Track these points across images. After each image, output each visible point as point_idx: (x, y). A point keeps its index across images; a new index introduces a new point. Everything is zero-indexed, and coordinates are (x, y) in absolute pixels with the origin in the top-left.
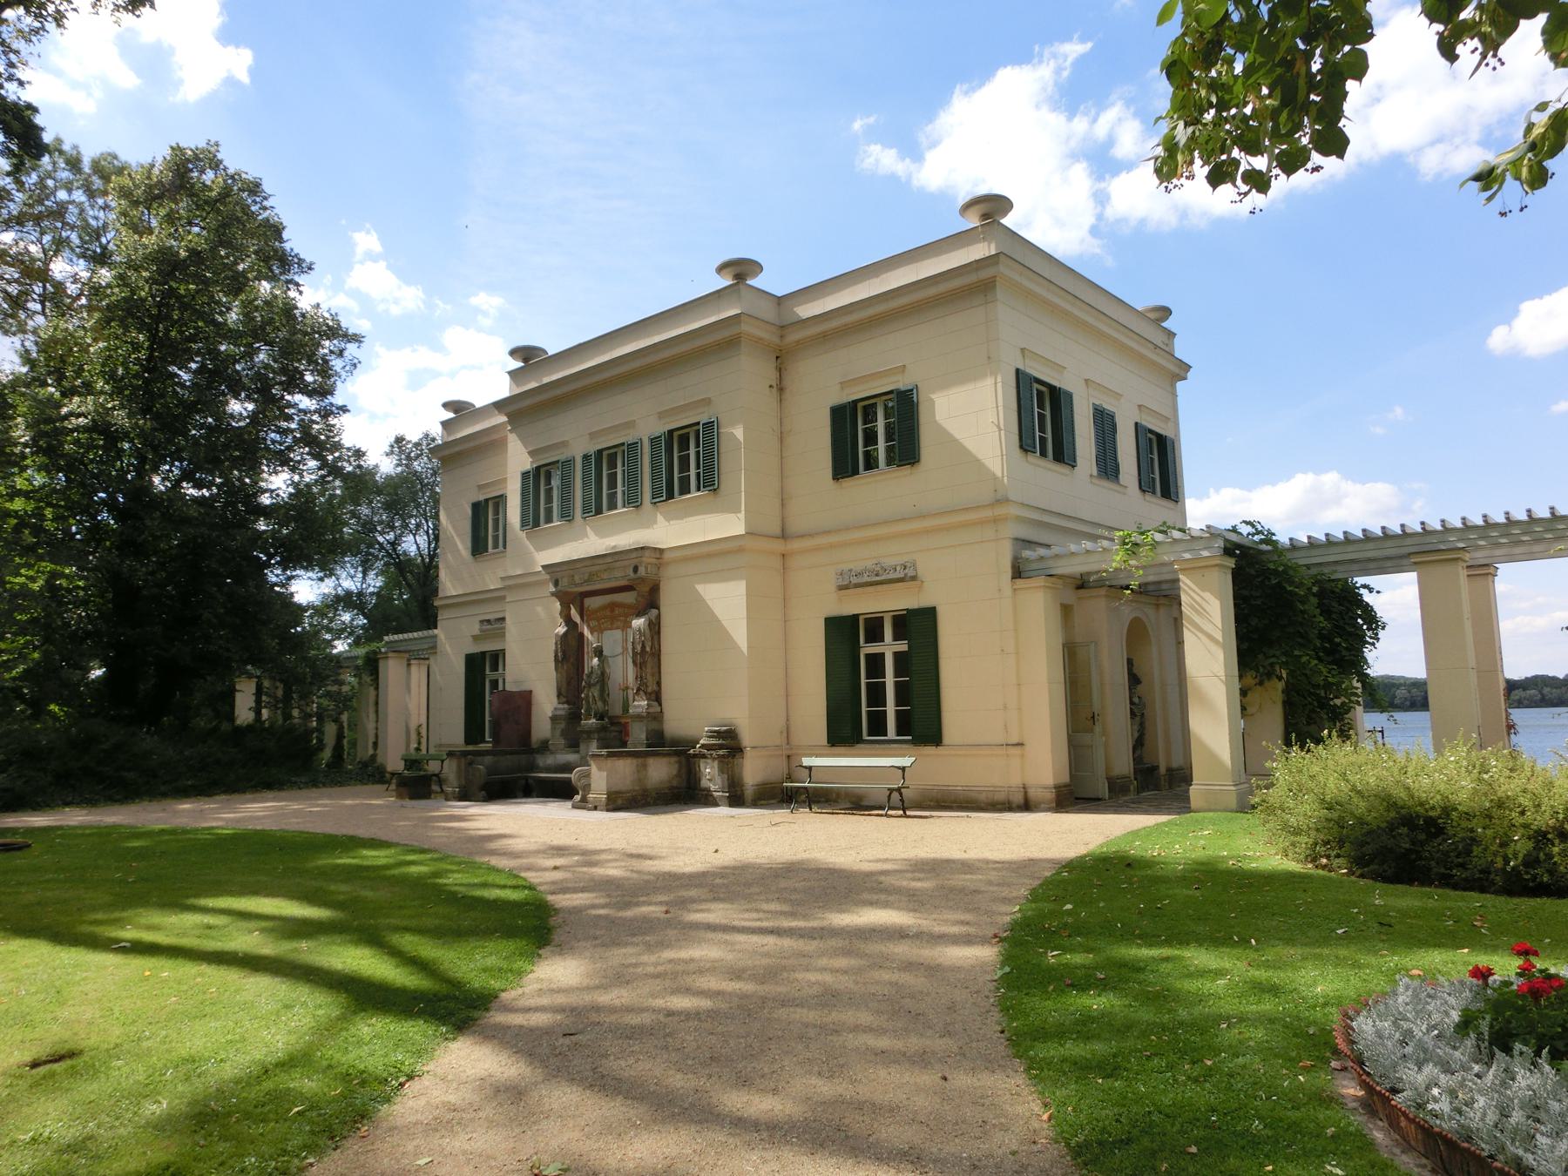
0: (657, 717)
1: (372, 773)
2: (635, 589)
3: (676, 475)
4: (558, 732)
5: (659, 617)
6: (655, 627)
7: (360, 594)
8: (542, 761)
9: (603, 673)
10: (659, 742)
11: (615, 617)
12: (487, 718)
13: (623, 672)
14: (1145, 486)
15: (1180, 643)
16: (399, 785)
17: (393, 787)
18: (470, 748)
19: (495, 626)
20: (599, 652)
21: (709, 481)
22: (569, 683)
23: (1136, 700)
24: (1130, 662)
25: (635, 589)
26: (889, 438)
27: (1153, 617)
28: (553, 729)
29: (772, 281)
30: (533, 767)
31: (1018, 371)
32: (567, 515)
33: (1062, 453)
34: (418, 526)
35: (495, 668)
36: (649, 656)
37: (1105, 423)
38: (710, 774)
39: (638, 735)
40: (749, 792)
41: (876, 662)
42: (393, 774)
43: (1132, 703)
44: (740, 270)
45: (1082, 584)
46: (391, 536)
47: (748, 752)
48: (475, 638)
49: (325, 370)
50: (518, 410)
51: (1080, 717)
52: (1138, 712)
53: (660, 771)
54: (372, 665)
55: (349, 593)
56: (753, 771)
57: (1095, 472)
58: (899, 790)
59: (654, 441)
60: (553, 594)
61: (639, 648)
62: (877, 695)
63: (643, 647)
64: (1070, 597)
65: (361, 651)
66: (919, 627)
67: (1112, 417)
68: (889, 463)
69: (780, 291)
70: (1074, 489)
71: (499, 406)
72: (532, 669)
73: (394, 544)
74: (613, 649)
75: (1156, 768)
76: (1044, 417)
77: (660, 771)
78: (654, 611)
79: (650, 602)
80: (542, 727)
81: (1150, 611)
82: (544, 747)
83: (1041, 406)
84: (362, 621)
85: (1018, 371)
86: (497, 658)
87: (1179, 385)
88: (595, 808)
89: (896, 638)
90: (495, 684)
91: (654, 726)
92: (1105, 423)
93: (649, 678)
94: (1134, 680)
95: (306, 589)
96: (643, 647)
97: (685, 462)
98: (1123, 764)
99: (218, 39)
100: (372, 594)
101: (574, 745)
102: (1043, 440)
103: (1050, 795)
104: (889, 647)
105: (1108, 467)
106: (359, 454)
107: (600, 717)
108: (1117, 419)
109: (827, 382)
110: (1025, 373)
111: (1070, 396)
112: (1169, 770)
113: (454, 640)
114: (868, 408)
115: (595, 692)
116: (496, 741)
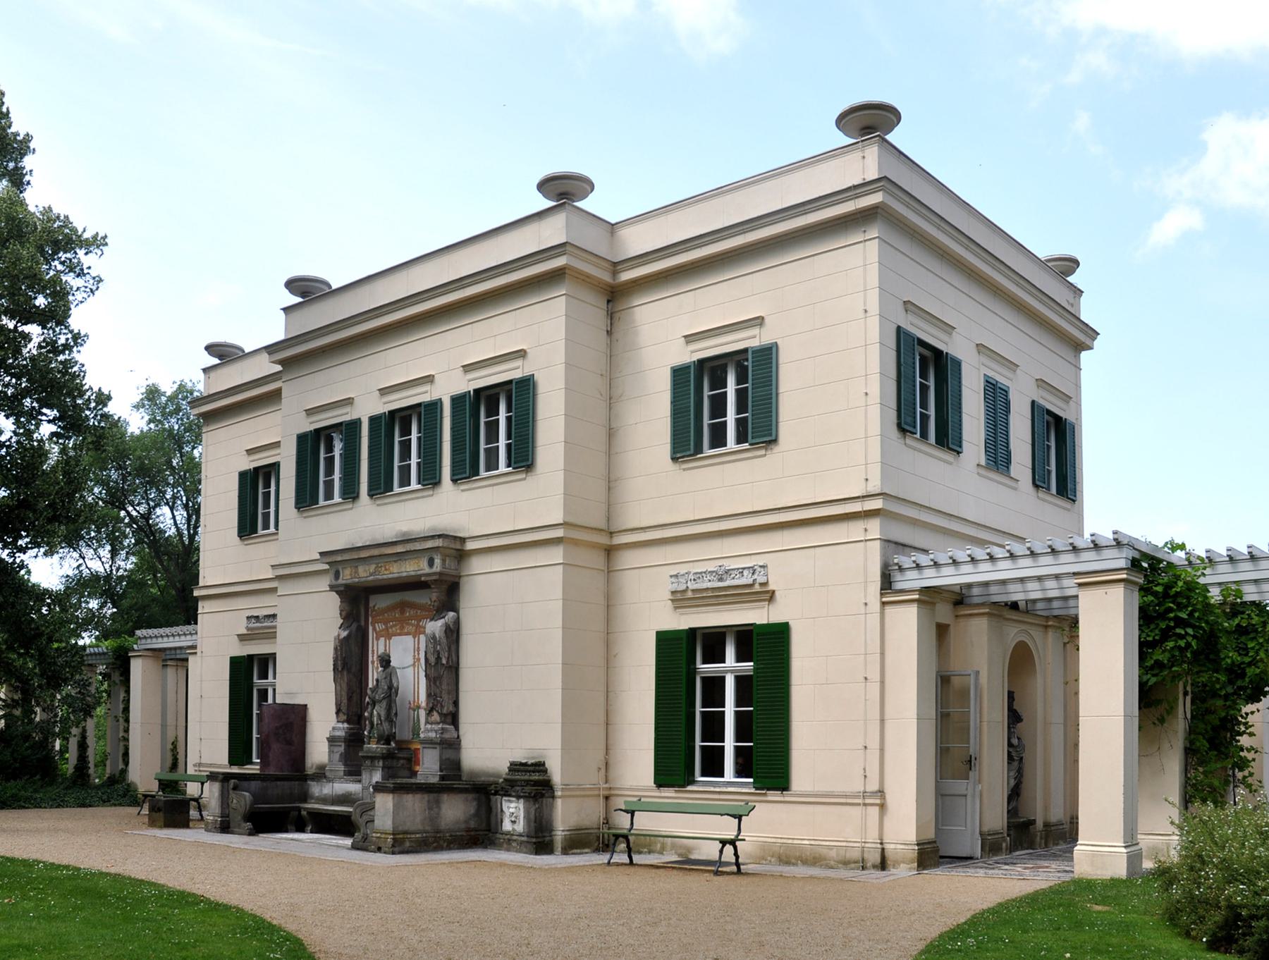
0: (451, 746)
1: (117, 791)
2: (428, 586)
4: (337, 756)
5: (457, 622)
6: (453, 633)
7: (108, 577)
8: (317, 789)
9: (390, 687)
10: (454, 777)
11: (405, 619)
12: (255, 735)
13: (413, 682)
14: (1039, 482)
16: (152, 809)
17: (145, 811)
18: (235, 770)
19: (262, 627)
20: (385, 661)
21: (522, 458)
22: (350, 699)
23: (1015, 741)
24: (1011, 696)
27: (1046, 646)
28: (331, 752)
30: (305, 797)
31: (899, 328)
32: (350, 493)
33: (948, 439)
34: (174, 497)
35: (264, 675)
36: (445, 669)
37: (996, 397)
38: (513, 815)
39: (429, 766)
41: (714, 687)
42: (146, 796)
43: (1010, 745)
44: (564, 189)
45: (959, 598)
46: (143, 509)
48: (242, 638)
49: (60, 295)
50: (296, 356)
51: (949, 755)
52: (1016, 756)
53: (455, 811)
54: (121, 663)
55: (95, 577)
56: (564, 816)
57: (983, 463)
58: (733, 842)
60: (332, 588)
61: (432, 660)
62: (714, 727)
63: (438, 659)
64: (944, 612)
65: (106, 645)
66: (768, 647)
67: (1006, 392)
68: (741, 438)
69: (613, 222)
70: (957, 483)
71: (271, 349)
72: (306, 678)
73: (146, 517)
74: (404, 655)
75: (1033, 822)
76: (925, 387)
77: (455, 811)
78: (451, 614)
79: (447, 593)
80: (319, 750)
81: (1036, 633)
82: (321, 774)
83: (924, 375)
84: (109, 610)
86: (265, 663)
87: (1084, 355)
88: (379, 849)
89: (740, 658)
90: (263, 694)
91: (449, 754)
92: (996, 397)
93: (445, 696)
94: (1014, 717)
95: (47, 570)
96: (438, 659)
97: (493, 425)
98: (997, 818)
99: (774, 441)
100: (121, 578)
101: (354, 772)
102: (925, 418)
103: (912, 851)
104: (731, 665)
105: (998, 457)
106: (103, 399)
107: (387, 739)
108: (1011, 396)
109: (670, 332)
110: (908, 334)
111: (957, 364)
112: (1047, 825)
113: (215, 639)
116: (264, 764)
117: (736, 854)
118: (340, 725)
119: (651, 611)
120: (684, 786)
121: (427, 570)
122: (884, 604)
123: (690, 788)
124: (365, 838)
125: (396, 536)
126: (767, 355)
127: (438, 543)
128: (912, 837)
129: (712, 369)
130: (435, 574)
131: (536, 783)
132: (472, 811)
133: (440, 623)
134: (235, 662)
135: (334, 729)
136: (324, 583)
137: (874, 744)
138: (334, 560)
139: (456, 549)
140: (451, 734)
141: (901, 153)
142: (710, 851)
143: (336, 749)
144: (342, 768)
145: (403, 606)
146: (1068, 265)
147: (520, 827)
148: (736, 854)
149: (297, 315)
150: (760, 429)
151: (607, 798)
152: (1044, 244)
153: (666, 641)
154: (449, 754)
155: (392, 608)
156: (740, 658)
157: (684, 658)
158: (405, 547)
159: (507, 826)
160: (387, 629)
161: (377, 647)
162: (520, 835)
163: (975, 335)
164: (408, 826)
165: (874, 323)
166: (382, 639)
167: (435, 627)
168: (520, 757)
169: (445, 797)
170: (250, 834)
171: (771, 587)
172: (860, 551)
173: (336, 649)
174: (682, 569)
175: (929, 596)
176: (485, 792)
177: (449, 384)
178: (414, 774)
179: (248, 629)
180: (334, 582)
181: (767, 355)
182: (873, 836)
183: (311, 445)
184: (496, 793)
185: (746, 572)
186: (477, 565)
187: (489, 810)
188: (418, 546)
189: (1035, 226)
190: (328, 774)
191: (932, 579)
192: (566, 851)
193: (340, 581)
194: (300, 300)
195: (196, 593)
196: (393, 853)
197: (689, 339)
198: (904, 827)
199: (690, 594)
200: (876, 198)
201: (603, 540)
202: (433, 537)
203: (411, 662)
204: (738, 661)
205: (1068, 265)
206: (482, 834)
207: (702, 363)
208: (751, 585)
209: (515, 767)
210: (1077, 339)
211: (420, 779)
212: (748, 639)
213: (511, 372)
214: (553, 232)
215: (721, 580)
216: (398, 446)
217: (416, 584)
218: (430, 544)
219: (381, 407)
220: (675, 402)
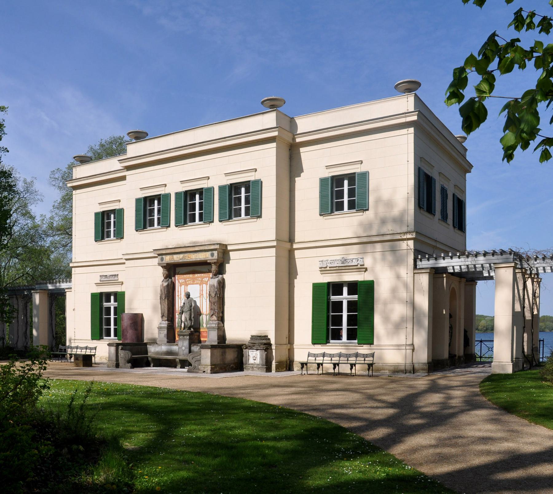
2: (216, 264)
6: (222, 285)
20: (188, 296)
28: (159, 333)
33: (430, 210)
59: (221, 188)
60: (159, 264)
68: (201, 219)
77: (230, 356)
78: (221, 276)
82: (154, 342)
104: (345, 297)
105: (444, 217)
118: (164, 322)
119: (310, 274)
120: (326, 344)
121: (210, 258)
122: (414, 273)
123: (328, 344)
125: (190, 243)
126: (365, 176)
127: (217, 247)
129: (337, 180)
130: (215, 259)
131: (265, 344)
132: (236, 356)
133: (216, 280)
134: (93, 296)
135: (160, 323)
136: (156, 261)
138: (160, 253)
141: (420, 100)
143: (162, 332)
144: (166, 340)
147: (258, 361)
153: (316, 287)
156: (341, 294)
157: (326, 294)
159: (251, 361)
160: (186, 282)
162: (258, 365)
166: (183, 286)
168: (255, 333)
170: (131, 368)
171: (365, 266)
173: (161, 291)
174: (325, 259)
178: (225, 343)
179: (100, 281)
180: (161, 262)
181: (365, 176)
185: (354, 260)
187: (242, 356)
190: (158, 342)
193: (164, 262)
195: (71, 265)
197: (328, 167)
198: (423, 356)
199: (328, 268)
203: (199, 295)
204: (349, 294)
207: (333, 177)
208: (326, 267)
209: (253, 337)
212: (353, 287)
215: (343, 263)
219: (183, 188)
220: (321, 192)
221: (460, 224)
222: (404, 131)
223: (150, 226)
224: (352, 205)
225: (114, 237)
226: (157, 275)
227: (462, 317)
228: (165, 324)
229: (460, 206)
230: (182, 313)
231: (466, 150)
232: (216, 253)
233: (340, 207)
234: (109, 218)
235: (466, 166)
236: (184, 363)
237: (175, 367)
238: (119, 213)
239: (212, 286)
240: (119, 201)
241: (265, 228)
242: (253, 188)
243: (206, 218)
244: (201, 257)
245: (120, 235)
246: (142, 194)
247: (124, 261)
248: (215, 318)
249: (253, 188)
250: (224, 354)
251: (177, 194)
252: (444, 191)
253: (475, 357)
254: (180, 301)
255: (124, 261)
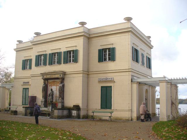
0: (63, 103)
2: (62, 78)
3: (68, 59)
4: (42, 104)
5: (64, 84)
6: (63, 86)
9: (53, 94)
10: (63, 108)
15: (16, 63)
20: (52, 90)
22: (45, 95)
25: (62, 78)
26: (73, 57)
29: (89, 26)
33: (137, 61)
38: (74, 113)
39: (59, 106)
40: (81, 117)
44: (83, 24)
47: (81, 110)
50: (35, 43)
53: (65, 112)
56: (82, 113)
59: (50, 54)
60: (42, 79)
61: (60, 90)
70: (138, 67)
74: (55, 88)
76: (136, 55)
77: (65, 112)
79: (63, 80)
85: (133, 47)
88: (55, 118)
91: (63, 104)
103: (136, 118)
105: (143, 64)
114: (105, 50)
115: (50, 97)
117: (111, 119)
121: (60, 77)
124: (52, 117)
127: (62, 73)
128: (136, 116)
136: (41, 77)
137: (130, 103)
138: (43, 74)
139: (64, 73)
140: (63, 101)
142: (108, 118)
145: (54, 82)
146: (149, 37)
147: (75, 115)
148: (111, 119)
149: (35, 38)
150: (112, 58)
151: (87, 111)
152: (147, 35)
154: (63, 104)
155: (53, 82)
158: (55, 73)
161: (49, 88)
163: (141, 47)
164: (59, 115)
165: (130, 46)
167: (61, 85)
168: (74, 104)
169: (64, 110)
172: (127, 77)
173: (43, 88)
174: (100, 78)
175: (139, 83)
176: (70, 110)
177: (63, 50)
182: (130, 116)
183: (38, 57)
184: (71, 110)
186: (67, 76)
188: (58, 73)
189: (146, 33)
191: (139, 80)
192: (82, 119)
194: (36, 36)
196: (58, 119)
200: (130, 30)
201: (87, 73)
202: (61, 72)
205: (149, 37)
206: (69, 116)
210: (151, 47)
211: (58, 108)
213: (74, 49)
214: (81, 30)
216: (53, 58)
217: (57, 78)
218: (60, 73)
221: (149, 66)
222: (80, 38)
223: (54, 64)
224: (109, 59)
225: (57, 63)
226: (41, 83)
227: (151, 99)
228: (43, 100)
229: (149, 60)
230: (49, 96)
231: (151, 41)
232: (61, 75)
233: (105, 60)
234: (27, 62)
235: (151, 47)
236: (49, 115)
237: (46, 116)
238: (31, 60)
239: (60, 87)
240: (31, 56)
241: (79, 67)
242: (75, 53)
243: (59, 63)
244: (56, 76)
245: (30, 68)
246: (37, 54)
247: (31, 77)
248: (61, 98)
249: (75, 53)
250: (63, 112)
251: (49, 54)
252: (142, 55)
253: (156, 114)
254: (49, 92)
255: (31, 77)
